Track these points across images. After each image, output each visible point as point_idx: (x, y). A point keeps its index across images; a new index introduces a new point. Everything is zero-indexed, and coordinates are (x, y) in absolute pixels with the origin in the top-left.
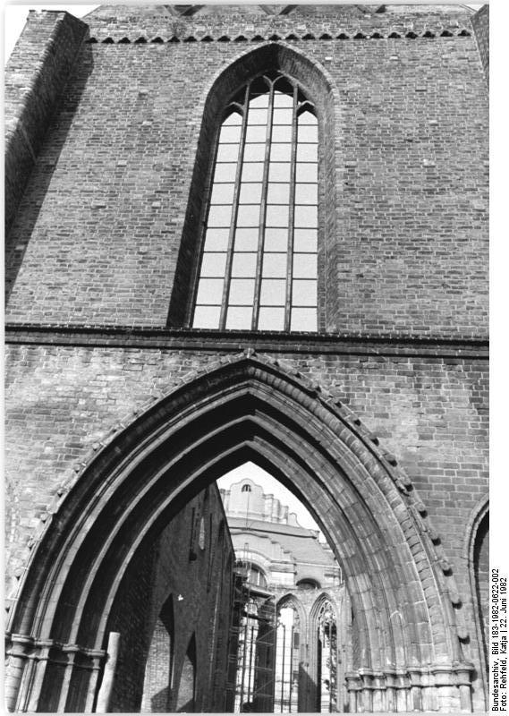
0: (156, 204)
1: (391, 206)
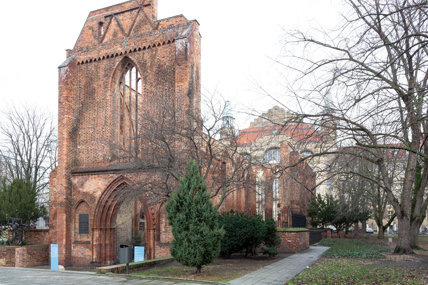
0: (104, 130)
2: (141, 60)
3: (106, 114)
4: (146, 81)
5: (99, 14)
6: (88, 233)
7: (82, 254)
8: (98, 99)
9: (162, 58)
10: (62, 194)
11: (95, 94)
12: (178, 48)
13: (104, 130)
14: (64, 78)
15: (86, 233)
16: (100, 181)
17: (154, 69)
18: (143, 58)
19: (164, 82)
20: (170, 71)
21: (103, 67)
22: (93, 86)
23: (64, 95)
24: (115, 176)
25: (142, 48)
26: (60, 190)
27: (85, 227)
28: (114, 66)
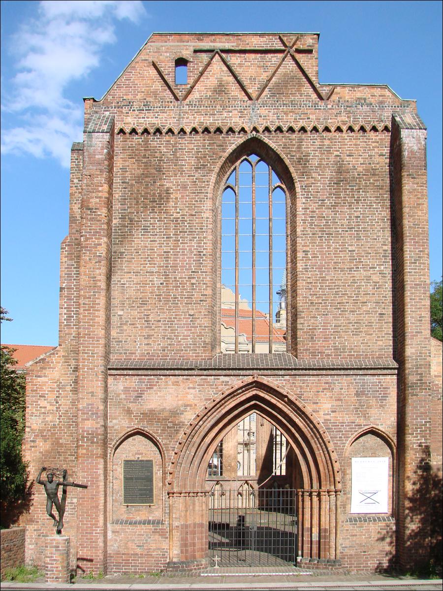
0: (193, 281)
1: (328, 280)
2: (295, 151)
3: (200, 247)
4: (308, 195)
5: (178, 42)
6: (152, 502)
7: (138, 546)
8: (179, 213)
9: (347, 156)
10: (92, 414)
11: (168, 202)
12: (410, 145)
13: (193, 281)
14: (100, 156)
15: (146, 503)
16: (192, 391)
17: (328, 173)
18: (298, 148)
19: (353, 203)
20: (365, 183)
21: (193, 149)
22: (163, 185)
23: (100, 194)
24: (237, 382)
25: (297, 129)
26: (88, 405)
27: (141, 490)
28: (225, 152)
